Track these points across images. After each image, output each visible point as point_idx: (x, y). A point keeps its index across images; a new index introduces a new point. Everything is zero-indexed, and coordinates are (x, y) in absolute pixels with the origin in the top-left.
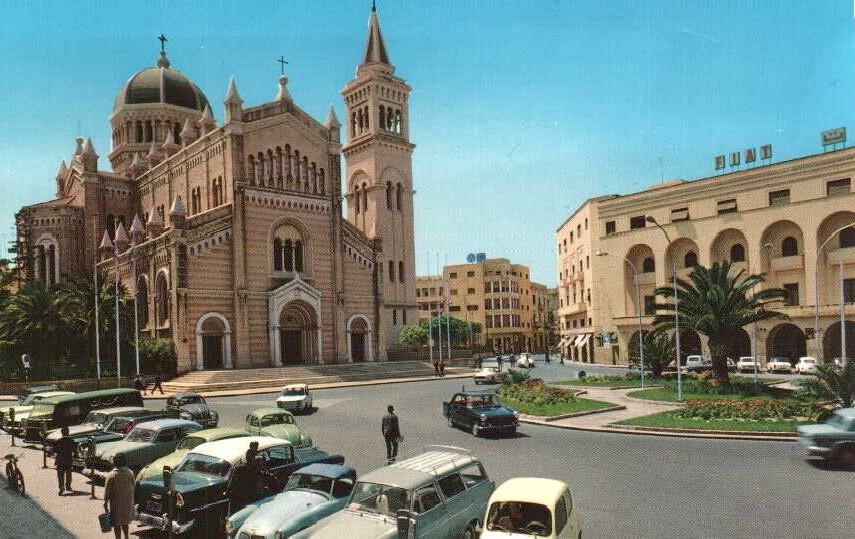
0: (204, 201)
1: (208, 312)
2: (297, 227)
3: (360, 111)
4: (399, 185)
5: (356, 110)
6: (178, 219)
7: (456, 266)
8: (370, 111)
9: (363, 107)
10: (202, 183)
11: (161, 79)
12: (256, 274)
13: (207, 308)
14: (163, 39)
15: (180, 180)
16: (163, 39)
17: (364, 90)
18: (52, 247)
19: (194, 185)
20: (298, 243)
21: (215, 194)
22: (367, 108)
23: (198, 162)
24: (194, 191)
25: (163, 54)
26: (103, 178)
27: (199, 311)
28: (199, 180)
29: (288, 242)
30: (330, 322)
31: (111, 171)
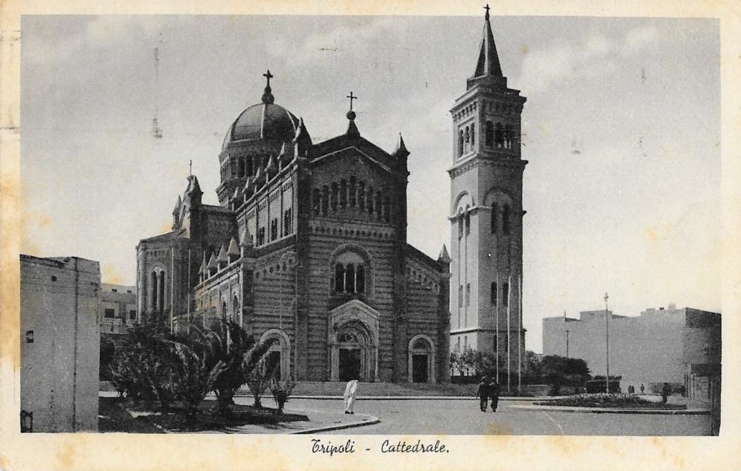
0: (266, 238)
1: (269, 329)
2: (363, 255)
3: (467, 128)
4: (506, 207)
5: (463, 128)
6: (249, 249)
7: (118, 286)
8: (477, 129)
9: (469, 124)
10: (278, 216)
11: (263, 118)
12: (388, 304)
13: (270, 325)
14: (269, 76)
15: (263, 213)
16: (269, 76)
17: (467, 109)
18: (163, 273)
19: (261, 226)
20: (360, 267)
21: (273, 231)
22: (473, 125)
23: (275, 197)
24: (273, 222)
25: (268, 90)
26: (212, 211)
27: (263, 328)
28: (276, 213)
29: (350, 266)
30: (79, 296)
31: (217, 204)
